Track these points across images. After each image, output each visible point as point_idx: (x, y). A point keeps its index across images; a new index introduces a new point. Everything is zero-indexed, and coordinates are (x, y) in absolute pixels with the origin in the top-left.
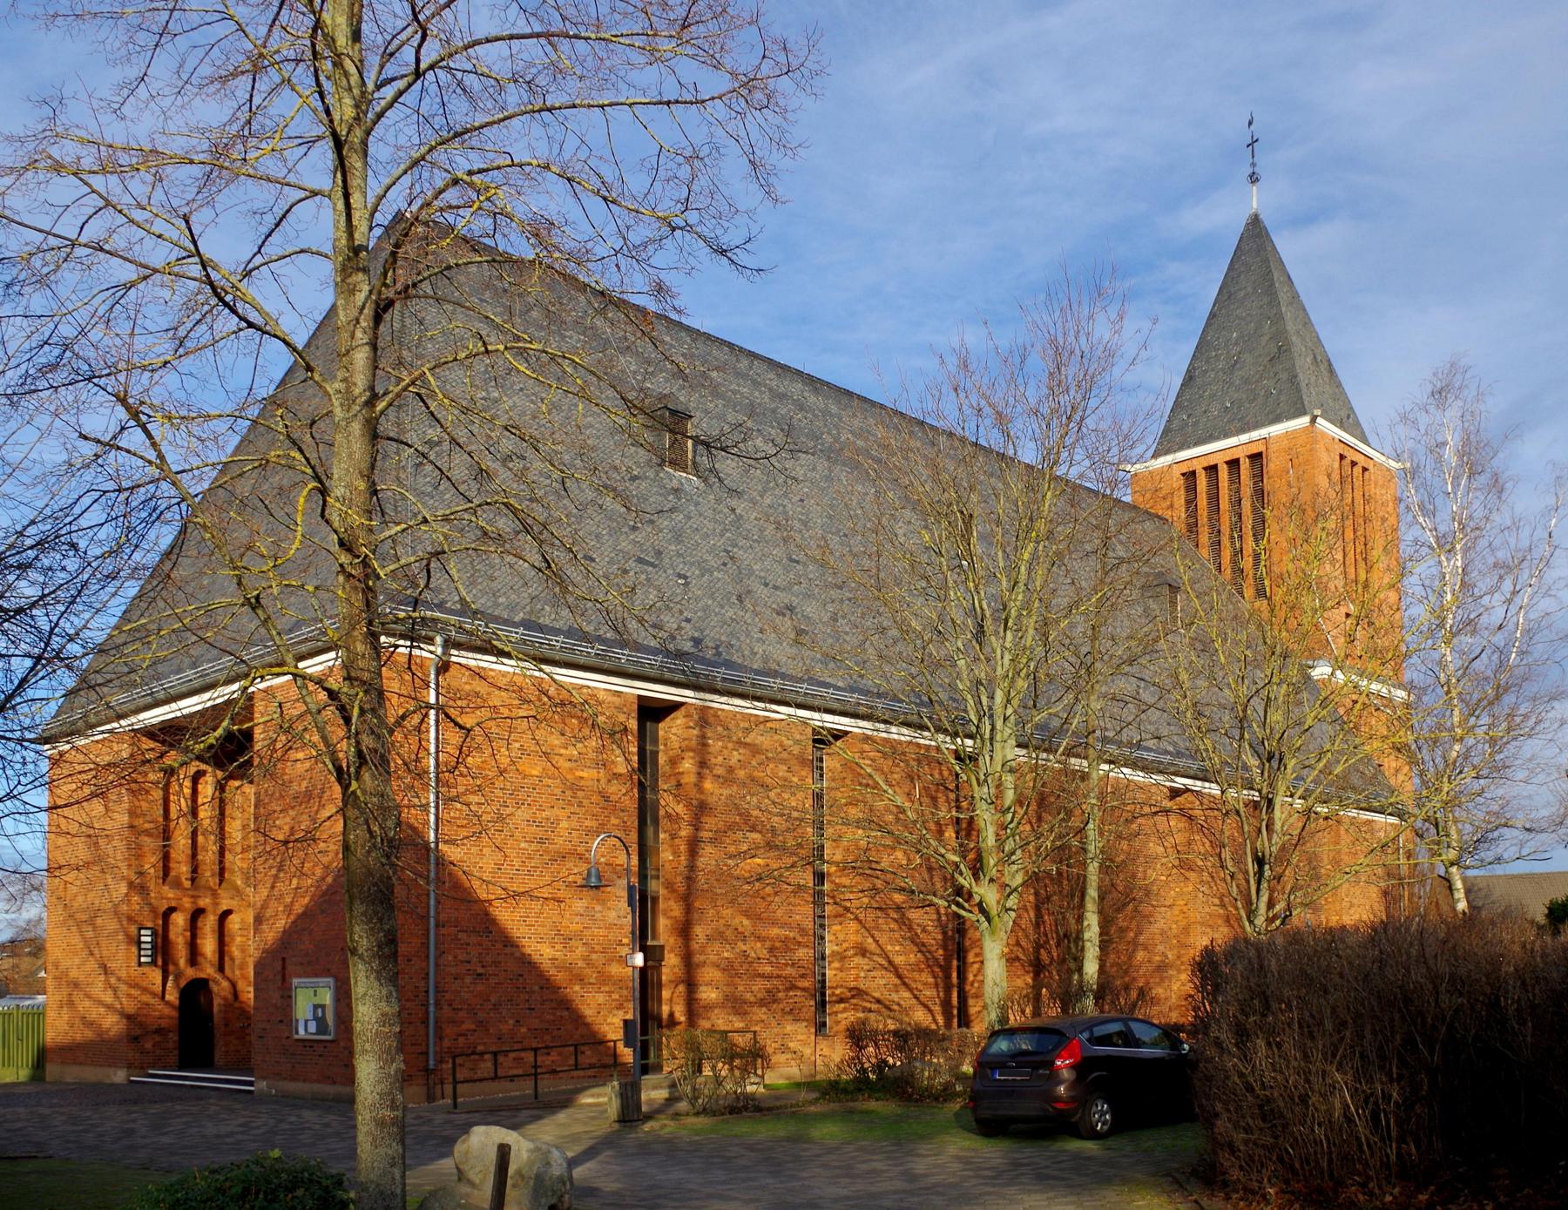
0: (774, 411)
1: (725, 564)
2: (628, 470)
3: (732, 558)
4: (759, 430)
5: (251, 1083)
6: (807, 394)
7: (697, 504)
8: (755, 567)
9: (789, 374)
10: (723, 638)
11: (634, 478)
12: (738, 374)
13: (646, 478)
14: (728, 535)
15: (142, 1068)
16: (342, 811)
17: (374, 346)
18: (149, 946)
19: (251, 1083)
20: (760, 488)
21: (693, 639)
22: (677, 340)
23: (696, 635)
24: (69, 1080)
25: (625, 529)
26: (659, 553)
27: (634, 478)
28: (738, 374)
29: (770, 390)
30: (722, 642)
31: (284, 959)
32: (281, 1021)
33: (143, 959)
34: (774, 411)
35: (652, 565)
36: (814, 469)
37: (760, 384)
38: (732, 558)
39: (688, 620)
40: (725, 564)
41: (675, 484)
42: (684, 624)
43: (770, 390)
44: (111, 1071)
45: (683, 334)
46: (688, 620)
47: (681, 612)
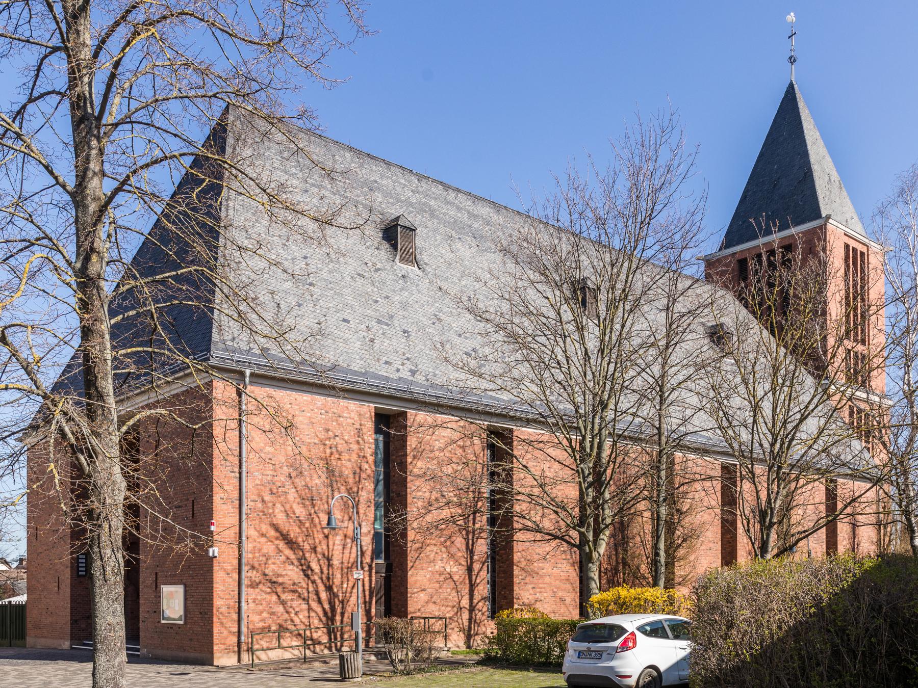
0: (470, 226)
1: (434, 324)
2: (374, 264)
3: (438, 319)
4: (460, 238)
5: (138, 650)
6: (491, 215)
7: (418, 285)
8: (453, 325)
9: (480, 202)
10: (430, 370)
11: (377, 270)
12: (448, 203)
13: (385, 270)
14: (436, 305)
15: (79, 640)
16: (827, 351)
17: (545, 324)
18: (84, 565)
19: (138, 650)
20: (459, 275)
21: (411, 371)
22: (409, 182)
23: (413, 368)
24: (39, 646)
25: (370, 302)
26: (392, 317)
27: (377, 270)
28: (448, 203)
29: (468, 212)
30: (430, 372)
31: (156, 573)
32: (155, 612)
33: (80, 573)
34: (470, 226)
35: (388, 325)
36: (494, 263)
37: (461, 208)
38: (438, 319)
39: (408, 359)
40: (434, 324)
41: (403, 273)
42: (405, 361)
43: (468, 212)
44: (61, 641)
45: (413, 178)
46: (408, 359)
47: (404, 354)
